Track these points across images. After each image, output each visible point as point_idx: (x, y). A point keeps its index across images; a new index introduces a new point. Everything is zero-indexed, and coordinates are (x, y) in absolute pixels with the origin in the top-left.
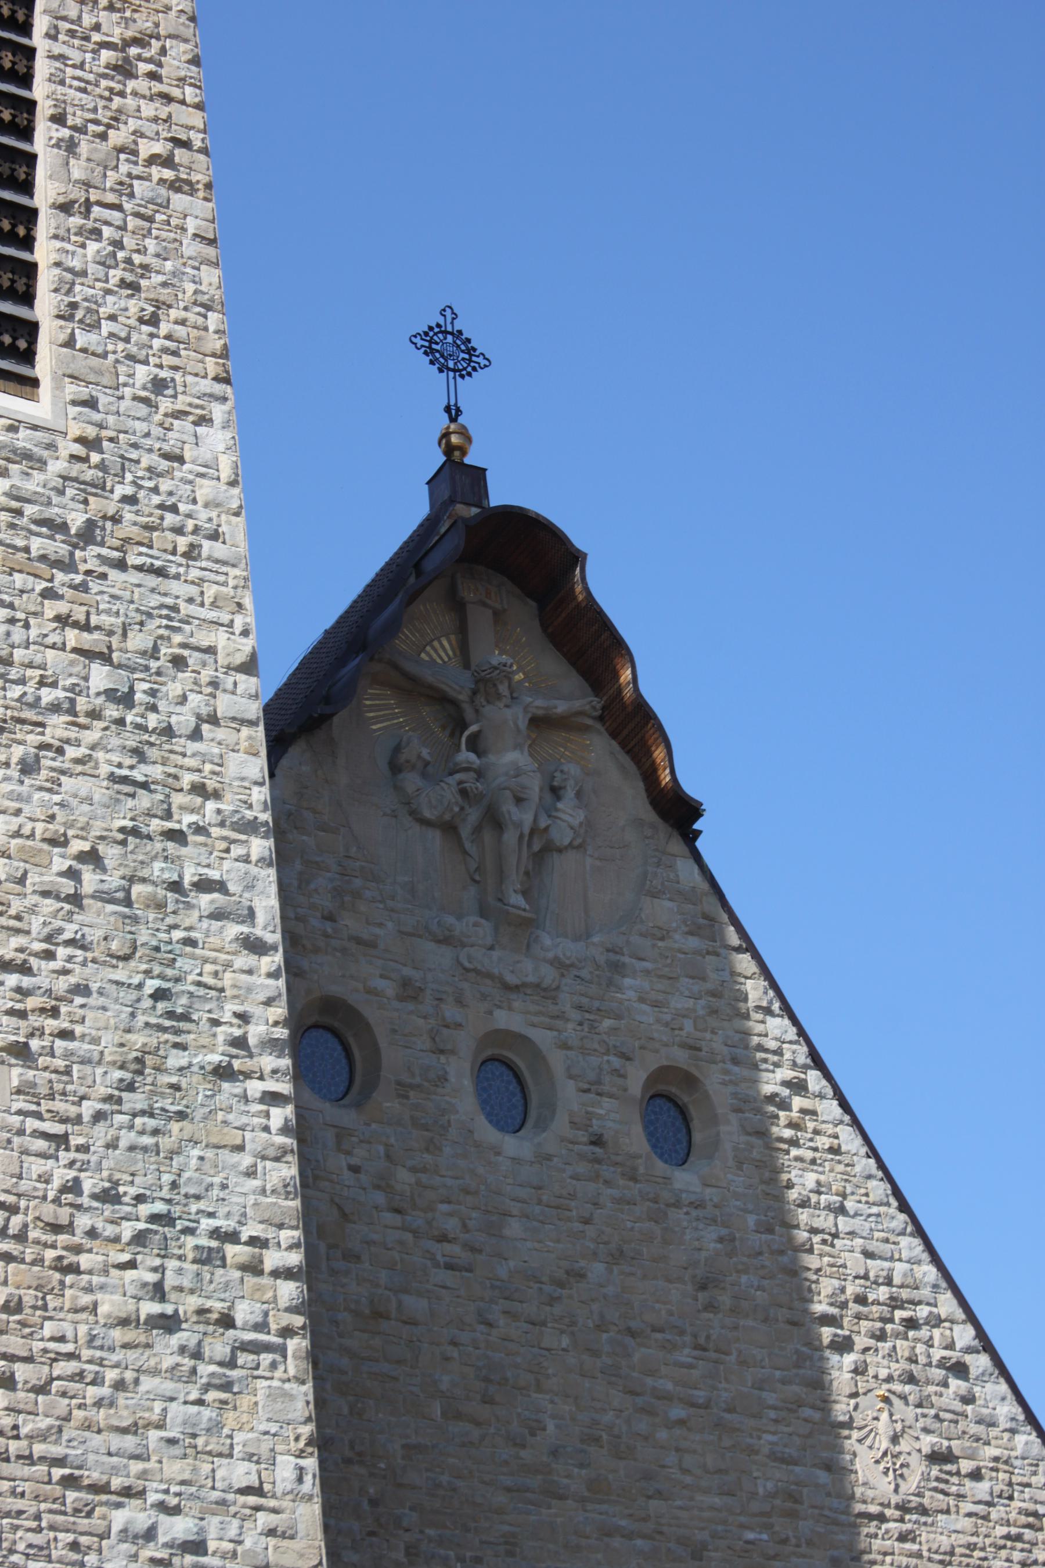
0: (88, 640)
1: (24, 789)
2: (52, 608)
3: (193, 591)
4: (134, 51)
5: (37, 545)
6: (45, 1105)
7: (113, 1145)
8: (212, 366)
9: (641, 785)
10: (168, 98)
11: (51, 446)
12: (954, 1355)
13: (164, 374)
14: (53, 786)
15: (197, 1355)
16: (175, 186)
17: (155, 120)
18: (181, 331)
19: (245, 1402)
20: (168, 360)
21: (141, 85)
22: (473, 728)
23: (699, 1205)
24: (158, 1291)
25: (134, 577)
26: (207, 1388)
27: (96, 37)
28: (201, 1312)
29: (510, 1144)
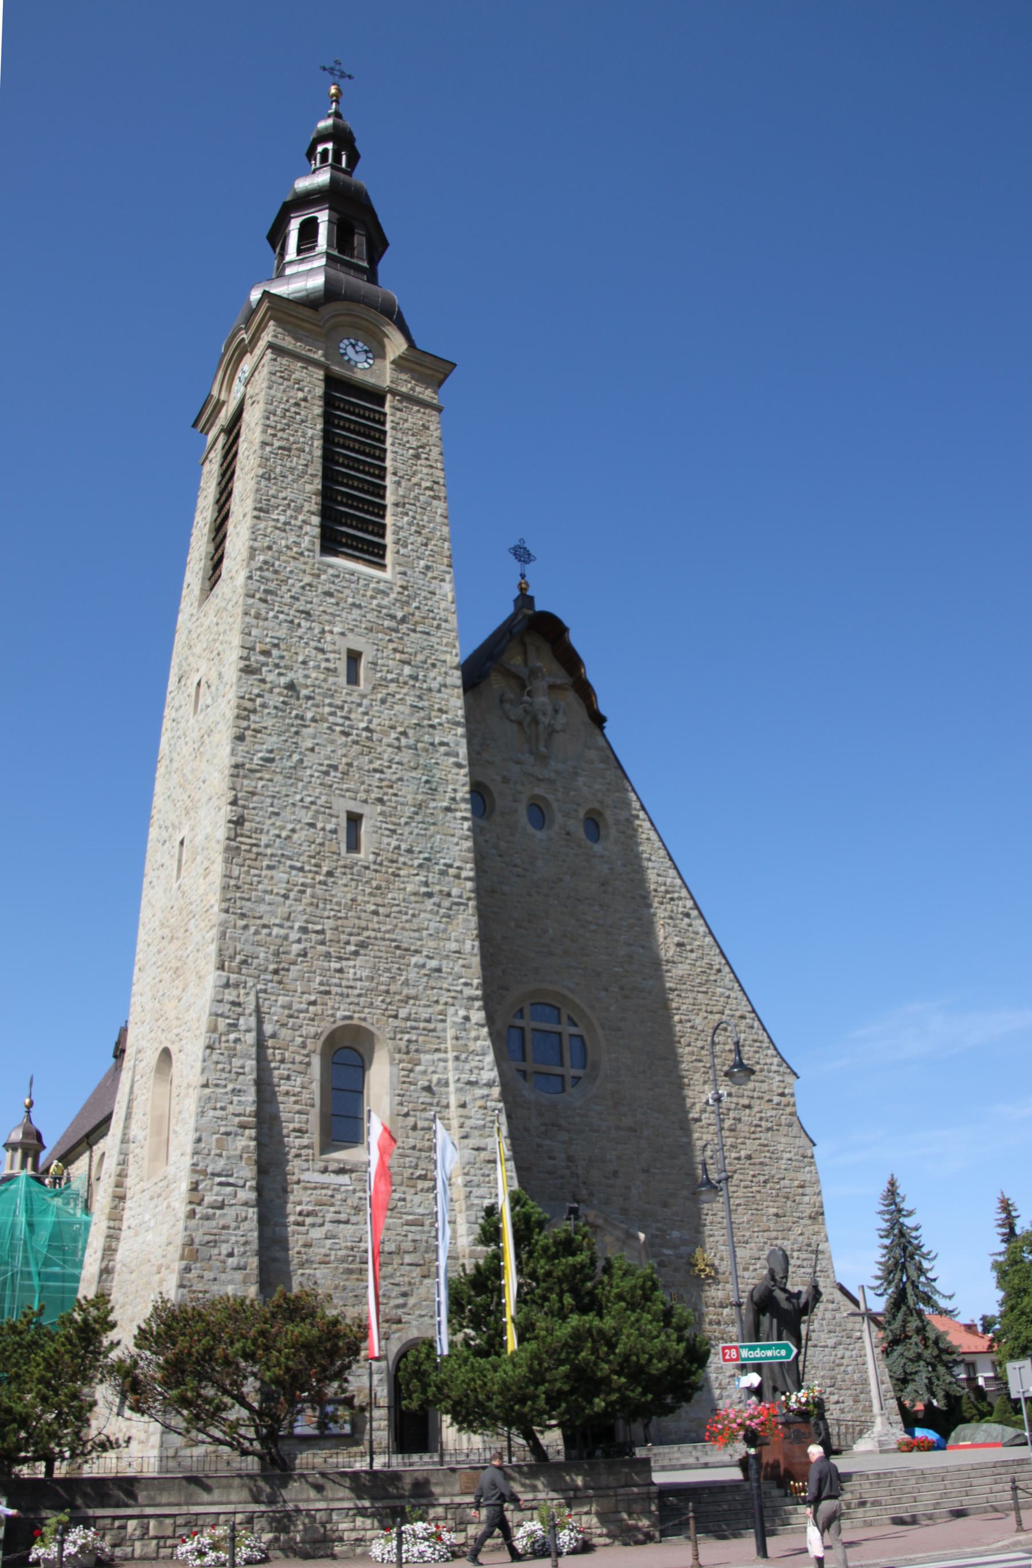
0: (404, 657)
1: (381, 709)
2: (391, 646)
3: (438, 640)
4: (420, 450)
5: (386, 623)
6: (389, 819)
7: (411, 833)
8: (446, 561)
9: (585, 710)
10: (431, 467)
11: (391, 589)
12: (686, 910)
13: (430, 564)
14: (391, 708)
15: (439, 906)
16: (434, 497)
17: (427, 474)
18: (435, 548)
19: (455, 922)
20: (431, 559)
21: (422, 462)
22: (529, 688)
23: (602, 857)
24: (426, 884)
25: (419, 635)
26: (442, 917)
27: (408, 445)
28: (441, 891)
29: (539, 834)
